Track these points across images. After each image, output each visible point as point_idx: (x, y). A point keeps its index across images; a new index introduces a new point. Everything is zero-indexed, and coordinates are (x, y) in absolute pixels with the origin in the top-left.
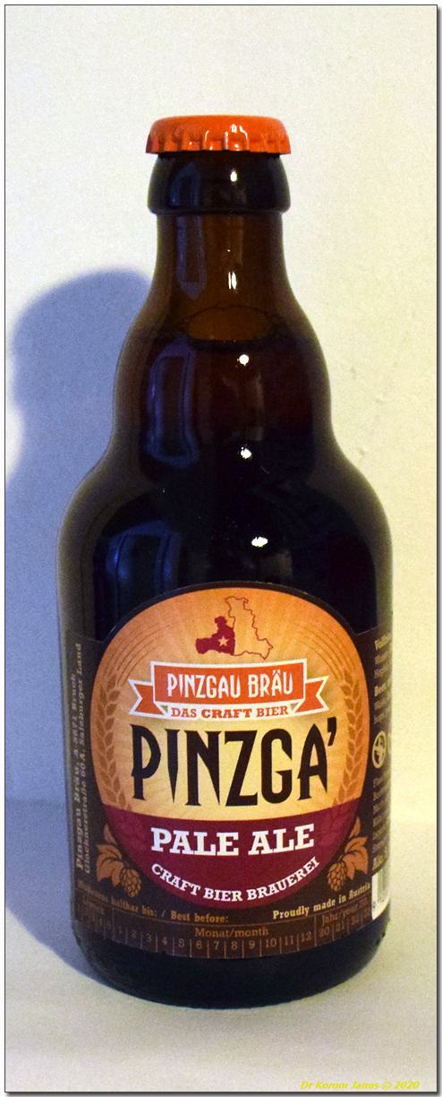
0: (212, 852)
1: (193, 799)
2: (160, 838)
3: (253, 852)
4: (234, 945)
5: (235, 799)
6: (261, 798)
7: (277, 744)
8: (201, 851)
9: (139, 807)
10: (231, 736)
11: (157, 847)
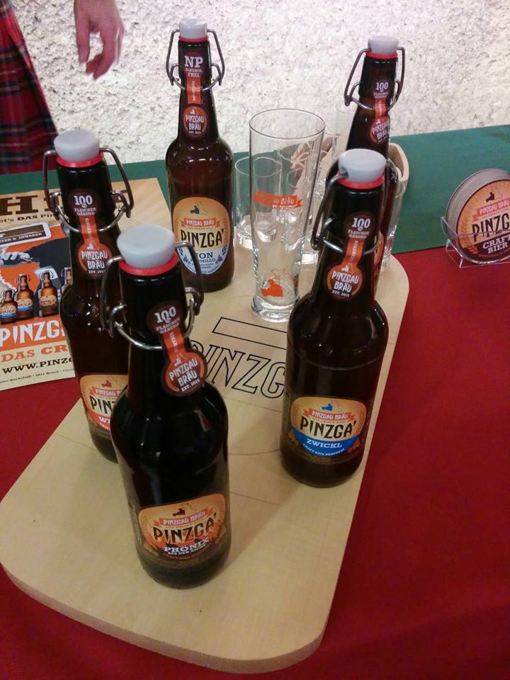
1: (315, 434)
7: (211, 235)
10: (201, 234)
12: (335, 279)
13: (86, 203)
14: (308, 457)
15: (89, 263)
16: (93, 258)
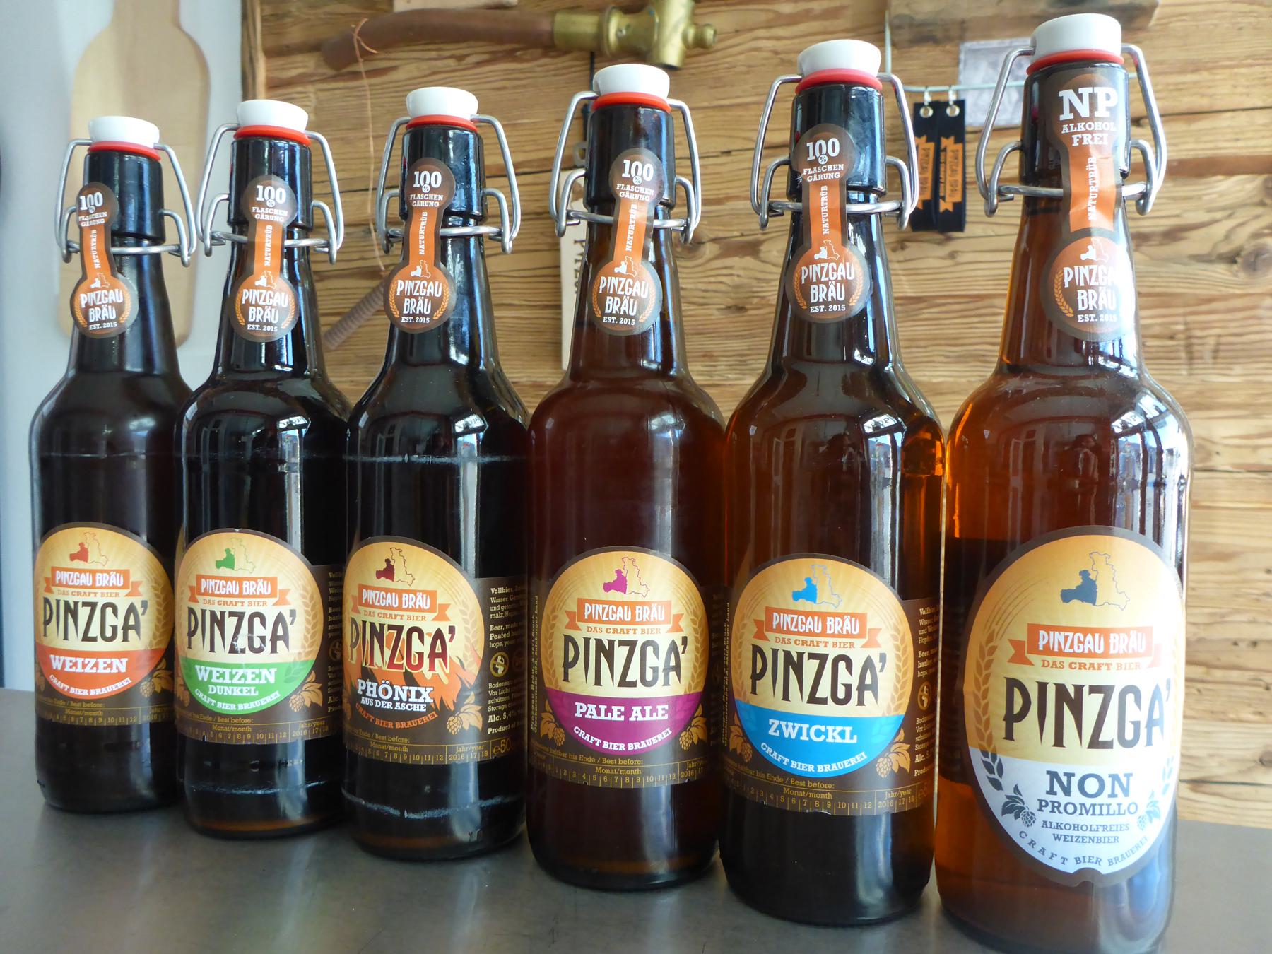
0: (609, 718)
1: (598, 683)
2: (580, 708)
3: (632, 719)
4: (605, 778)
5: (623, 683)
6: (639, 683)
8: (602, 717)
9: (568, 688)
11: (578, 714)
12: (248, 304)
13: (827, 154)
14: (581, 768)
15: (252, 310)
16: (261, 303)
